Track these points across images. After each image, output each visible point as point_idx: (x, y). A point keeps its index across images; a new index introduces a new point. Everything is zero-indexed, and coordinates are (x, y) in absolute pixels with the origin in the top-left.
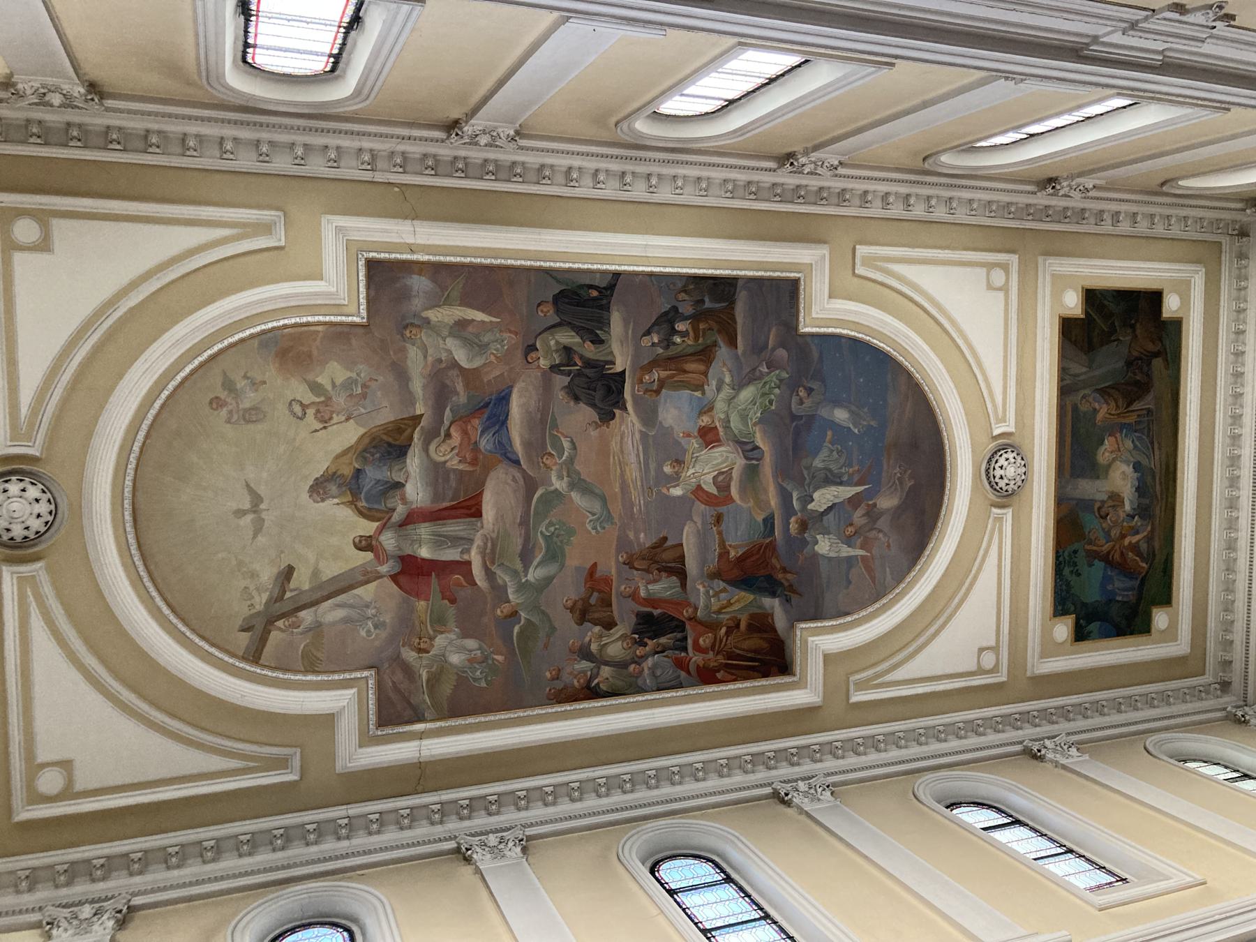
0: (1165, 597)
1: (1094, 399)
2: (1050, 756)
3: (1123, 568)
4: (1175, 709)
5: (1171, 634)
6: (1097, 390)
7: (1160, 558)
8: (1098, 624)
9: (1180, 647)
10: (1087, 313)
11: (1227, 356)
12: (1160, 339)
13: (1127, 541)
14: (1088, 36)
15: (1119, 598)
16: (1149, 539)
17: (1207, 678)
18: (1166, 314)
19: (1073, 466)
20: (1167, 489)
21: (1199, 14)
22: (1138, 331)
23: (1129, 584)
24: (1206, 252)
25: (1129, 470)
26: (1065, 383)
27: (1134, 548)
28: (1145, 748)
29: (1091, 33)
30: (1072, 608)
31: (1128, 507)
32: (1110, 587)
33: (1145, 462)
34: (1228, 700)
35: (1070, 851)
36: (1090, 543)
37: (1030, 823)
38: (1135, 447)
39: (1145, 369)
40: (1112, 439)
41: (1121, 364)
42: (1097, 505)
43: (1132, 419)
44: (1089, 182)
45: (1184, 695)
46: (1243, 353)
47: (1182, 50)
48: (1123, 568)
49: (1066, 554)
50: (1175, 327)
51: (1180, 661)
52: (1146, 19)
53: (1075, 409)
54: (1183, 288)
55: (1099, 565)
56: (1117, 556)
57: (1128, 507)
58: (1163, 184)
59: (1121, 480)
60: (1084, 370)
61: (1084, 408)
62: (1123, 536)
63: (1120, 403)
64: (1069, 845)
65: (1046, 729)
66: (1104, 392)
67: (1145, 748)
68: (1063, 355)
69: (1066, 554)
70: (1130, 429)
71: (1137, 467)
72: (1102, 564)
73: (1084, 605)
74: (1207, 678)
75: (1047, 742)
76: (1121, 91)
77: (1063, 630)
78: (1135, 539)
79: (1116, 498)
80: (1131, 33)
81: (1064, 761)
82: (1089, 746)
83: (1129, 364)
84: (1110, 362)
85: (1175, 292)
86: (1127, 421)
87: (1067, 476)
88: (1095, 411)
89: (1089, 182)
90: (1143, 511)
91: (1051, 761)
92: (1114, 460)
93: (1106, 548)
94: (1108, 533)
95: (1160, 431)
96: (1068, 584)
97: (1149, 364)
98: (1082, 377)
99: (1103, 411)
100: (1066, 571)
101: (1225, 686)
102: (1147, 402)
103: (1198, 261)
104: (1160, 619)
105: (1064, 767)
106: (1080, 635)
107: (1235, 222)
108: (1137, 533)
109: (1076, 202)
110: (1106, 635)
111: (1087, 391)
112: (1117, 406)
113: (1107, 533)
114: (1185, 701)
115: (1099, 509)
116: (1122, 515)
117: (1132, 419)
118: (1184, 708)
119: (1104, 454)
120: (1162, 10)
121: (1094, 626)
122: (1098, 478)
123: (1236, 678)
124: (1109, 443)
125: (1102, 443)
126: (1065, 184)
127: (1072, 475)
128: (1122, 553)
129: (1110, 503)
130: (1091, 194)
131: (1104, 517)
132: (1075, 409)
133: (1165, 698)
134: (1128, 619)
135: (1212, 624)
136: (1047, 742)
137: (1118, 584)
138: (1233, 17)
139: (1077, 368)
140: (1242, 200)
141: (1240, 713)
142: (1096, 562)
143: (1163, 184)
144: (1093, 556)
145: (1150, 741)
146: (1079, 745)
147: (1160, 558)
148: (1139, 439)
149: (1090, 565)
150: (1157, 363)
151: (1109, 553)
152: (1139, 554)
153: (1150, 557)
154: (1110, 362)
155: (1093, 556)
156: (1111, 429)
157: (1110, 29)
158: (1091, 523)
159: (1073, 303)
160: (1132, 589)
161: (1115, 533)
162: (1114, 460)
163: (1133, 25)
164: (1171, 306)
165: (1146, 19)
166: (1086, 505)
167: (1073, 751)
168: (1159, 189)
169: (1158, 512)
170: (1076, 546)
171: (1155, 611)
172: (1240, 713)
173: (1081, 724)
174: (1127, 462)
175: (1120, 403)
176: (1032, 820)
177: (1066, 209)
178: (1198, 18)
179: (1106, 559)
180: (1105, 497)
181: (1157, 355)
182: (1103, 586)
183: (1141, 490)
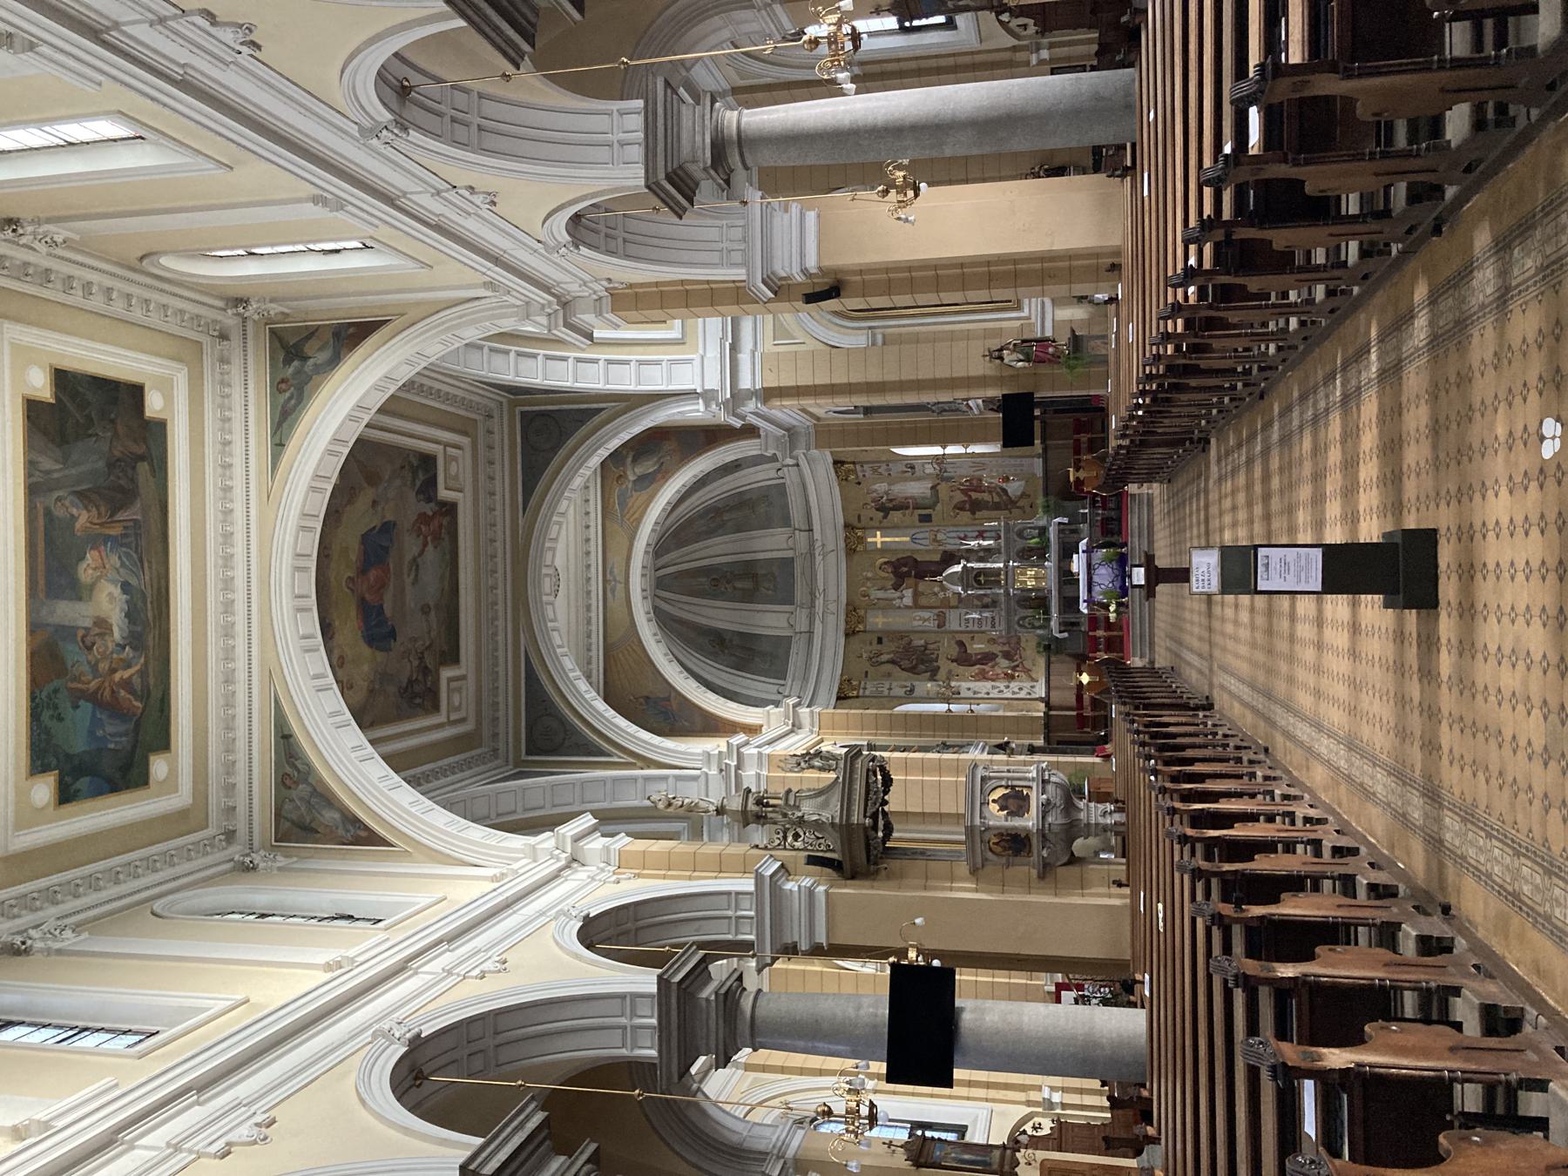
0: (163, 743)
1: (72, 503)
2: (39, 945)
3: (115, 710)
4: (178, 870)
5: (171, 785)
6: (75, 493)
7: (156, 694)
8: (87, 779)
9: (182, 798)
10: (57, 398)
11: (215, 469)
12: (145, 440)
13: (117, 676)
14: (107, 18)
15: (112, 746)
16: (143, 673)
17: (210, 832)
18: (148, 413)
19: (49, 584)
20: (160, 613)
21: (229, 30)
22: (121, 429)
23: (122, 728)
24: (188, 353)
25: (117, 591)
26: (34, 479)
27: (127, 684)
28: (153, 913)
29: (114, 17)
30: (54, 762)
31: (117, 634)
32: (100, 733)
33: (133, 581)
34: (235, 851)
35: (86, 1029)
36: (75, 679)
37: (27, 1020)
38: (123, 564)
39: (130, 472)
40: (95, 553)
41: (101, 464)
42: (81, 633)
43: (115, 531)
44: (60, 233)
45: (187, 853)
46: (230, 466)
47: (206, 70)
48: (115, 710)
49: (44, 694)
50: (156, 431)
51: (183, 814)
52: (175, 17)
53: (48, 513)
54: (166, 387)
55: (86, 707)
56: (107, 693)
57: (117, 634)
58: (142, 258)
59: (108, 603)
60: (58, 467)
61: (59, 512)
62: (114, 671)
63: (103, 509)
64: (81, 1024)
65: (27, 919)
66: (84, 497)
67: (153, 913)
68: (30, 445)
69: (44, 694)
70: (117, 542)
71: (126, 587)
72: (89, 705)
73: (68, 757)
74: (210, 832)
75: (32, 933)
76: (122, 115)
77: (43, 790)
78: (126, 674)
79: (102, 624)
80: (159, 27)
81: (57, 945)
82: (92, 925)
83: (112, 465)
84: (89, 460)
85: (158, 389)
86: (112, 532)
87: (42, 595)
88: (74, 518)
89: (60, 233)
90: (135, 640)
91: (41, 951)
92: (99, 578)
93: (93, 685)
94: (94, 667)
95: (146, 545)
96: (47, 731)
97: (134, 468)
98: (56, 475)
99: (83, 518)
100: (46, 715)
101: (230, 835)
102: (132, 513)
103: (180, 360)
104: (159, 767)
105: (59, 952)
106: (65, 796)
107: (215, 321)
108: (129, 666)
109: (40, 258)
110: (97, 793)
111: (61, 493)
112: (99, 514)
113: (94, 667)
114: (189, 859)
115: (83, 637)
116: (111, 646)
117: (115, 531)
118: (187, 867)
119: (86, 571)
120: (192, 13)
121: (83, 783)
122: (80, 599)
123: (241, 828)
124: (91, 558)
125: (83, 558)
126: (30, 229)
127: (48, 596)
128: (113, 692)
129: (97, 630)
130: (59, 251)
131: (90, 648)
132: (48, 513)
133: (169, 859)
134: (125, 773)
135: (213, 765)
136: (32, 933)
137: (110, 729)
138: (259, 47)
139: (47, 464)
140: (221, 298)
141: (247, 860)
142: (82, 703)
143: (142, 258)
144: (78, 696)
145: (157, 906)
146: (77, 928)
147: (156, 694)
148: (128, 555)
149: (76, 707)
150: (143, 467)
151: (96, 692)
152: (132, 692)
153: (145, 695)
154: (89, 460)
155: (78, 696)
156: (96, 541)
157: (138, 17)
158: (72, 653)
159: (40, 385)
160: (126, 734)
161: (104, 666)
162: (99, 578)
163: (162, 20)
164: (154, 404)
165: (175, 17)
166: (67, 632)
167: (68, 933)
168: (136, 264)
169: (151, 643)
170: (56, 683)
171: (152, 758)
172: (247, 860)
173: (71, 905)
174: (113, 582)
175: (103, 509)
176: (28, 1015)
177: (26, 264)
178: (228, 35)
179: (93, 697)
180: (88, 623)
181: (142, 458)
182: (91, 733)
183: (131, 615)
